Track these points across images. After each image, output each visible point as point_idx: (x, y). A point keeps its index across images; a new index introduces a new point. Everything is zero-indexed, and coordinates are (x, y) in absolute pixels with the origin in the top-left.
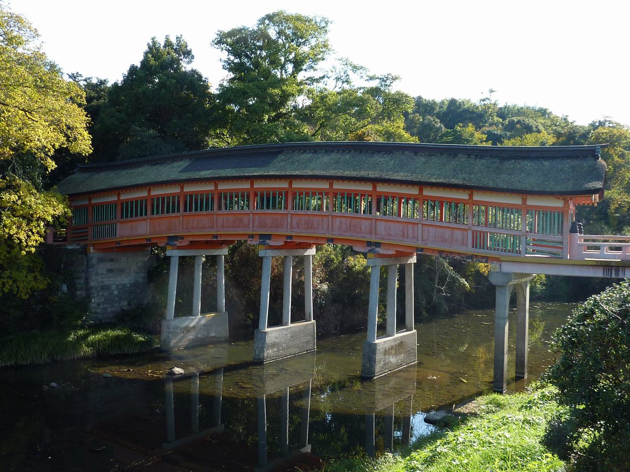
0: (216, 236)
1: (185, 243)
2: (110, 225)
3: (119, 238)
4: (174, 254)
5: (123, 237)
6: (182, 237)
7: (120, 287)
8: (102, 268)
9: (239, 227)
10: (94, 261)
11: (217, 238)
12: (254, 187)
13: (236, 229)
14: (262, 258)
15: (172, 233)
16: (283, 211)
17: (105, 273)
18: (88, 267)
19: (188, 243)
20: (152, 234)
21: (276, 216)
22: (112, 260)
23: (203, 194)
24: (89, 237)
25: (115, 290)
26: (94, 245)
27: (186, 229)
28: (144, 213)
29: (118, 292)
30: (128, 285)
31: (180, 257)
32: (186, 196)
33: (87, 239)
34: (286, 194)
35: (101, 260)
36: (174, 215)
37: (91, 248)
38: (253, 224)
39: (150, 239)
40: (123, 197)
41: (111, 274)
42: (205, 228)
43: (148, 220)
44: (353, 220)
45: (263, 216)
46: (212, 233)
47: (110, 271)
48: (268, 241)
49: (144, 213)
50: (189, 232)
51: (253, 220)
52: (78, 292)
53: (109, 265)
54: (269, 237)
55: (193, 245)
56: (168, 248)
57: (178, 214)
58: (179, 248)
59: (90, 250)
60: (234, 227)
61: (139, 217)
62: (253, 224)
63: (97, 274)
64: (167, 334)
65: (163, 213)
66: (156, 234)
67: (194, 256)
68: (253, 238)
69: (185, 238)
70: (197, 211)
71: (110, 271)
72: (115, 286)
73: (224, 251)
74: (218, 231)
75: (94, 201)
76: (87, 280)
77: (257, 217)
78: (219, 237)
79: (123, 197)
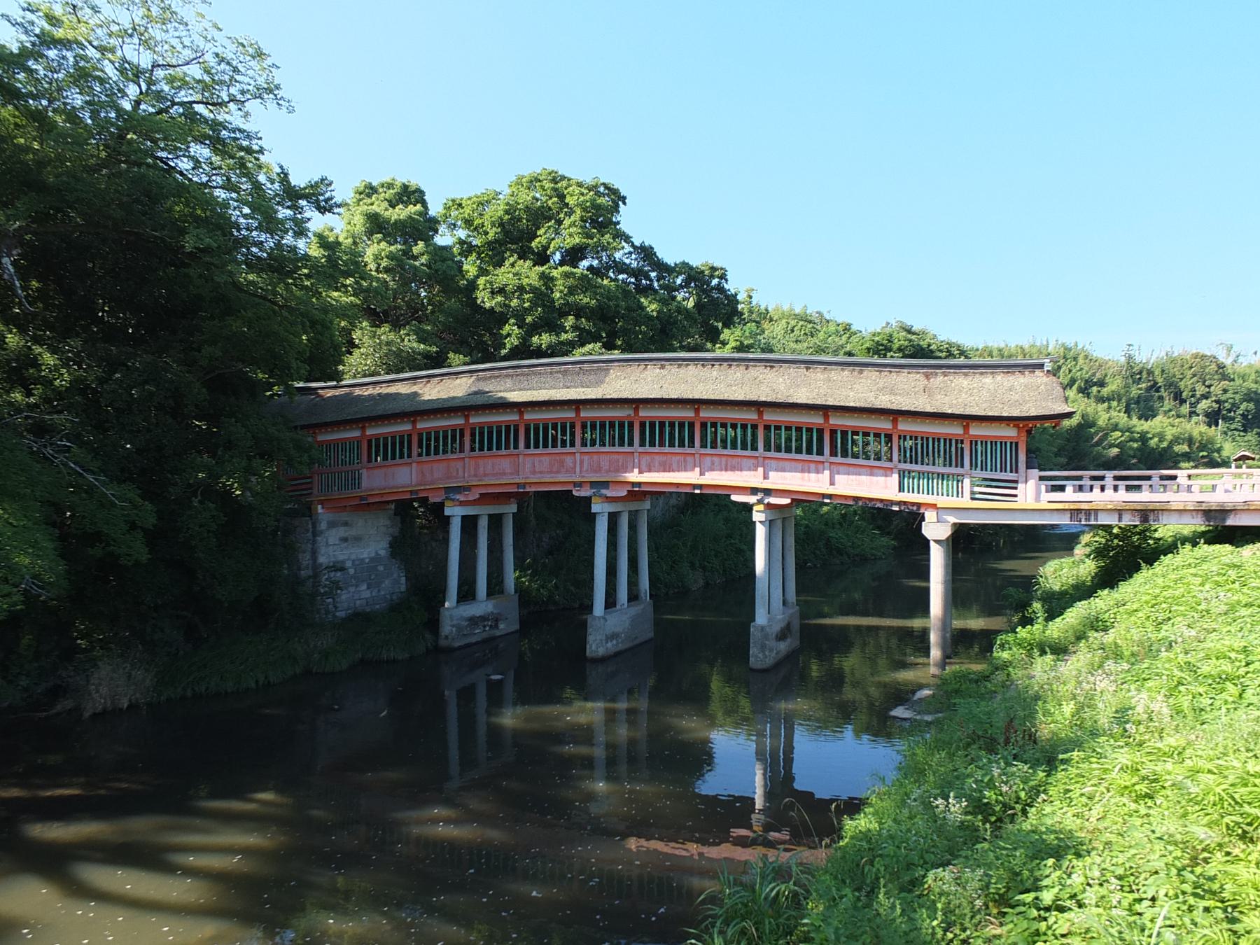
0: (524, 485)
1: (474, 495)
2: (919, 442)
3: (365, 491)
4: (455, 512)
5: (373, 490)
6: (468, 488)
7: (357, 563)
8: (334, 536)
9: (558, 472)
10: (323, 526)
11: (524, 488)
12: (418, 427)
13: (553, 475)
14: (449, 517)
15: (454, 483)
16: (626, 449)
17: (337, 543)
18: (315, 534)
19: (478, 496)
20: (421, 485)
21: (615, 456)
22: (346, 524)
23: (484, 428)
24: (315, 491)
25: (351, 568)
26: (322, 502)
27: (475, 475)
28: (406, 455)
29: (356, 570)
30: (367, 560)
31: (463, 517)
32: (420, 435)
33: (311, 493)
34: (573, 426)
35: (332, 525)
36: (455, 456)
37: (320, 507)
38: (581, 467)
39: (417, 492)
40: (422, 425)
41: (345, 544)
42: (504, 474)
43: (414, 465)
44: (730, 459)
45: (595, 457)
46: (517, 481)
47: (345, 540)
48: (604, 492)
49: (406, 455)
50: (479, 480)
51: (582, 462)
52: (302, 572)
53: (342, 532)
54: (605, 484)
55: (485, 498)
56: (447, 503)
57: (462, 455)
58: (462, 503)
59: (317, 511)
60: (551, 472)
61: (398, 461)
62: (581, 467)
63: (327, 545)
64: (450, 628)
65: (490, 449)
66: (429, 485)
67: (477, 515)
68: (581, 487)
69: (473, 490)
70: (510, 449)
71: (345, 540)
72: (351, 562)
73: (647, 505)
74: (526, 478)
75: (320, 438)
76: (314, 553)
77: (586, 458)
78: (527, 487)
79: (370, 432)
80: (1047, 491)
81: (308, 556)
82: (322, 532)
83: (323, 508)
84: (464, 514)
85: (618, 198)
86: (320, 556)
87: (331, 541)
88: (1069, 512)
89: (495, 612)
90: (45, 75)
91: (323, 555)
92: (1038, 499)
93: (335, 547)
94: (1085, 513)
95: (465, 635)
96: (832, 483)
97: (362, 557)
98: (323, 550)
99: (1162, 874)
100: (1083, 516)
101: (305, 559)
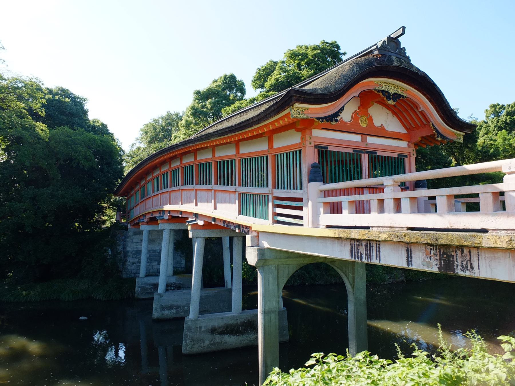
63: (132, 242)
80: (325, 213)
81: (121, 247)
82: (129, 237)
83: (131, 226)
84: (207, 236)
85: (198, 93)
86: (128, 247)
87: (135, 241)
88: (348, 243)
89: (177, 282)
90: (467, 270)
91: (129, 247)
92: (316, 223)
93: (138, 244)
94: (366, 246)
95: (148, 293)
96: (215, 208)
97: (155, 249)
98: (129, 245)
99: (491, 361)
100: (362, 250)
101: (120, 248)
